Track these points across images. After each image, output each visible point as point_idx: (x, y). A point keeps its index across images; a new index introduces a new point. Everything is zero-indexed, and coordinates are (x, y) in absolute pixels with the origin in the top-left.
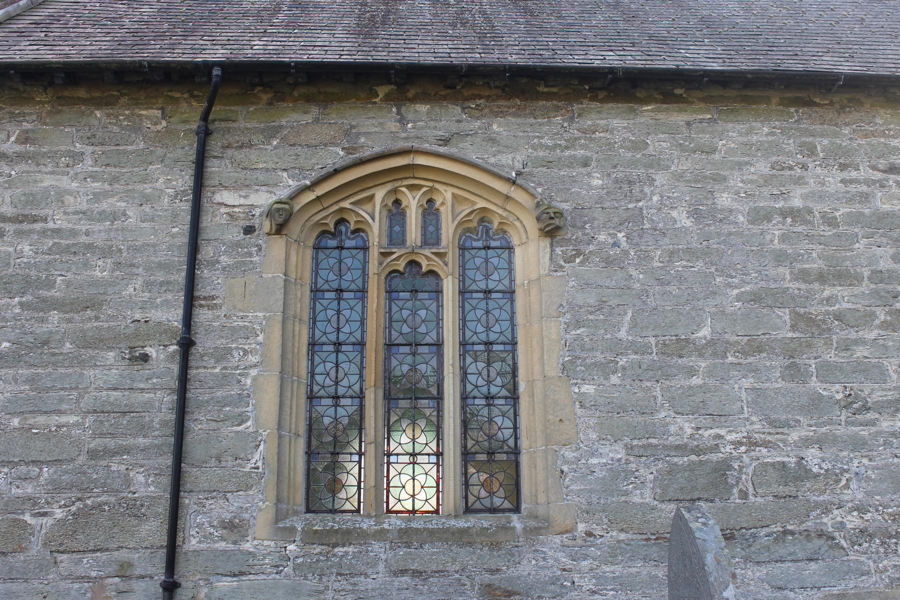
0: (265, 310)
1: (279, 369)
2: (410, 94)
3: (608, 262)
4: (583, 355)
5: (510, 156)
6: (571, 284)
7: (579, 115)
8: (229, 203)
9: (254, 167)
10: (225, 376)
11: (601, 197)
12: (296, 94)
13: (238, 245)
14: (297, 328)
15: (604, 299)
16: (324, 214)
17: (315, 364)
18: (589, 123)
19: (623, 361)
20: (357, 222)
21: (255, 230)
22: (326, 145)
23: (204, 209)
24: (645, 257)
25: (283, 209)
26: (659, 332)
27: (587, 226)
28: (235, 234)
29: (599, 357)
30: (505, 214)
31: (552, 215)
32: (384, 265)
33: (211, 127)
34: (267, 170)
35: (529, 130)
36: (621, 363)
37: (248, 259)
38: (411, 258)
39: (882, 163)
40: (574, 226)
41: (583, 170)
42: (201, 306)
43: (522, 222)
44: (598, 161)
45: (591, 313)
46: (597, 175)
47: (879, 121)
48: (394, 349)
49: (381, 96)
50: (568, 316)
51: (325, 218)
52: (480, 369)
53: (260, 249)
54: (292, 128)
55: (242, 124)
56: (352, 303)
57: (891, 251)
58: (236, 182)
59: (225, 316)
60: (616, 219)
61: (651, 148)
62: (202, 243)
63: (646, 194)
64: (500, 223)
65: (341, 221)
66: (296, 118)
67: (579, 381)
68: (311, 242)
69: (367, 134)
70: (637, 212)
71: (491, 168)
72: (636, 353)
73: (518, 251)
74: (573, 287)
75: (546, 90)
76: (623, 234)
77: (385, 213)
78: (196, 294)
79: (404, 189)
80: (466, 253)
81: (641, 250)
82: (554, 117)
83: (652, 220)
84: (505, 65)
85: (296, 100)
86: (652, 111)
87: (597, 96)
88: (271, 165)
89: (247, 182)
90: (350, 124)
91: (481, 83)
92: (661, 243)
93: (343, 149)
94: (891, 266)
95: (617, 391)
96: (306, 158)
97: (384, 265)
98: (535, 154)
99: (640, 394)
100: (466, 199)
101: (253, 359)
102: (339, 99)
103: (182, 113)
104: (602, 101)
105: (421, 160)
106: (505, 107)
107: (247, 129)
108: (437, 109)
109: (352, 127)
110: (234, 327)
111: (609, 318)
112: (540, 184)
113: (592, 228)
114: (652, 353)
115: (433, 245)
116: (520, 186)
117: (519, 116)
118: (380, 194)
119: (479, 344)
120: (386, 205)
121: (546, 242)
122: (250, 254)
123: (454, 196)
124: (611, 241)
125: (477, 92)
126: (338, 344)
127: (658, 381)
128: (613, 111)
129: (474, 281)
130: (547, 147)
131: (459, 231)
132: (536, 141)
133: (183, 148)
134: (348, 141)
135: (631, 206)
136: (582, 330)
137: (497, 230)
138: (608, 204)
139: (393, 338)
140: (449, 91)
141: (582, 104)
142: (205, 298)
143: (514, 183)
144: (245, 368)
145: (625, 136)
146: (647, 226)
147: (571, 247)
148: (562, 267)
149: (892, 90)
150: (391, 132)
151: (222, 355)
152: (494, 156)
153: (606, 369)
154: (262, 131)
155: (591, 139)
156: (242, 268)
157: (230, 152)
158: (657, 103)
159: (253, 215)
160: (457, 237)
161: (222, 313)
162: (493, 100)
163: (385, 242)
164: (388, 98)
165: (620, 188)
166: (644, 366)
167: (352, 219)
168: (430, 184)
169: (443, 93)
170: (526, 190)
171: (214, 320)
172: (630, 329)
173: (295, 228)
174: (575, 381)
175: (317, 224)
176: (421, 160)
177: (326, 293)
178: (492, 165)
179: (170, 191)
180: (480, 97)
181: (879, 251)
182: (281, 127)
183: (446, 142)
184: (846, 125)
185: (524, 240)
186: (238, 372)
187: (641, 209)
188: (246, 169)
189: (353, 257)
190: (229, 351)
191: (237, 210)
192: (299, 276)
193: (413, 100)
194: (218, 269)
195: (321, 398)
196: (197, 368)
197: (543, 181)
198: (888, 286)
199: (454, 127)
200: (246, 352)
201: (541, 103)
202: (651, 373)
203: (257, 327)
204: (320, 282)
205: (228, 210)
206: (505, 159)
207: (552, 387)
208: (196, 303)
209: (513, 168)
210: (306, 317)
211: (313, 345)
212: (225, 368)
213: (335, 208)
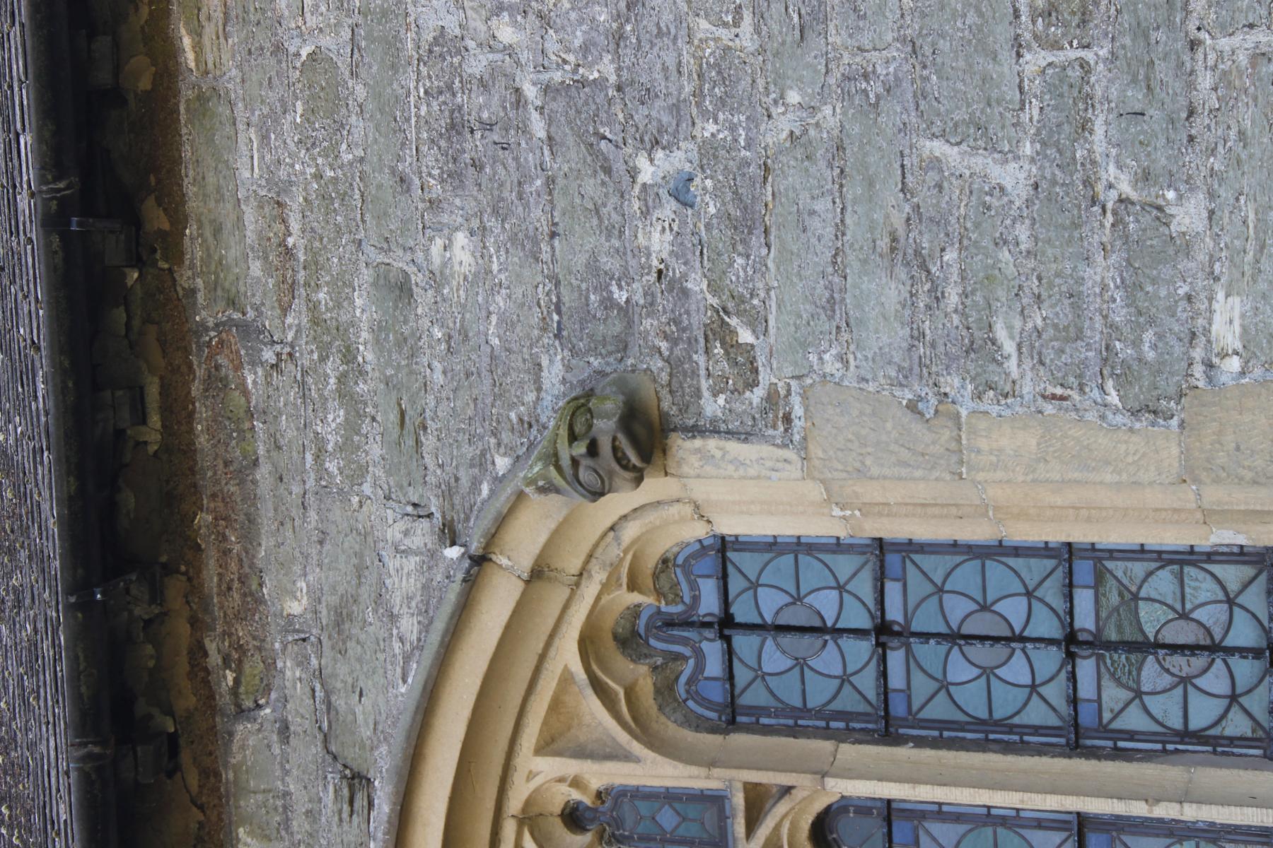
3: (746, 223)
4: (1095, 332)
5: (392, 563)
6: (831, 366)
7: (232, 303)
11: (513, 238)
15: (884, 244)
18: (256, 268)
19: (1119, 181)
24: (721, 79)
26: (1002, 34)
27: (621, 296)
29: (1102, 271)
30: (599, 574)
31: (580, 449)
35: (297, 489)
36: (1126, 188)
40: (623, 347)
41: (424, 300)
43: (624, 517)
44: (386, 245)
45: (937, 297)
46: (436, 248)
50: (951, 383)
52: (1167, 680)
60: (591, 187)
61: (327, 41)
63: (493, 69)
64: (633, 586)
67: (1198, 354)
70: (559, 105)
71: (440, 625)
72: (1085, 126)
73: (729, 526)
74: (842, 359)
75: (155, 420)
76: (642, 162)
80: (746, 700)
81: (698, 94)
82: (246, 393)
83: (585, 49)
84: (69, 608)
86: (197, 33)
87: (163, 235)
91: (149, 649)
92: (667, 17)
95: (1236, 208)
98: (380, 472)
99: (1247, 116)
100: (556, 705)
104: (179, 218)
106: (223, 565)
108: (249, 804)
111: (954, 228)
112: (482, 462)
113: (625, 278)
114: (1083, 64)
115: (723, 819)
116: (492, 538)
117: (251, 520)
119: (1073, 677)
121: (683, 448)
123: (546, 747)
124: (669, 208)
125: (183, 665)
127: (1194, 45)
128: (211, 179)
129: (845, 679)
130: (351, 427)
131: (672, 729)
132: (332, 466)
135: (538, 127)
136: (1001, 333)
137: (659, 593)
138: (537, 213)
140: (185, 757)
141: (193, 292)
143: (480, 561)
145: (292, 139)
146: (606, 68)
147: (700, 359)
148: (772, 398)
152: (393, 618)
153: (1148, 246)
155: (314, 265)
158: (167, 13)
160: (689, 736)
162: (206, 605)
165: (477, 165)
166: (1136, 98)
168: (509, 828)
169: (193, 780)
170: (502, 521)
172: (991, 147)
174: (1198, 370)
178: (426, 628)
180: (198, 651)
183: (357, 781)
185: (688, 509)
187: (547, 89)
197: (469, 451)
199: (307, 751)
201: (202, 441)
202: (1163, 71)
206: (403, 579)
207: (1221, 458)
209: (433, 555)
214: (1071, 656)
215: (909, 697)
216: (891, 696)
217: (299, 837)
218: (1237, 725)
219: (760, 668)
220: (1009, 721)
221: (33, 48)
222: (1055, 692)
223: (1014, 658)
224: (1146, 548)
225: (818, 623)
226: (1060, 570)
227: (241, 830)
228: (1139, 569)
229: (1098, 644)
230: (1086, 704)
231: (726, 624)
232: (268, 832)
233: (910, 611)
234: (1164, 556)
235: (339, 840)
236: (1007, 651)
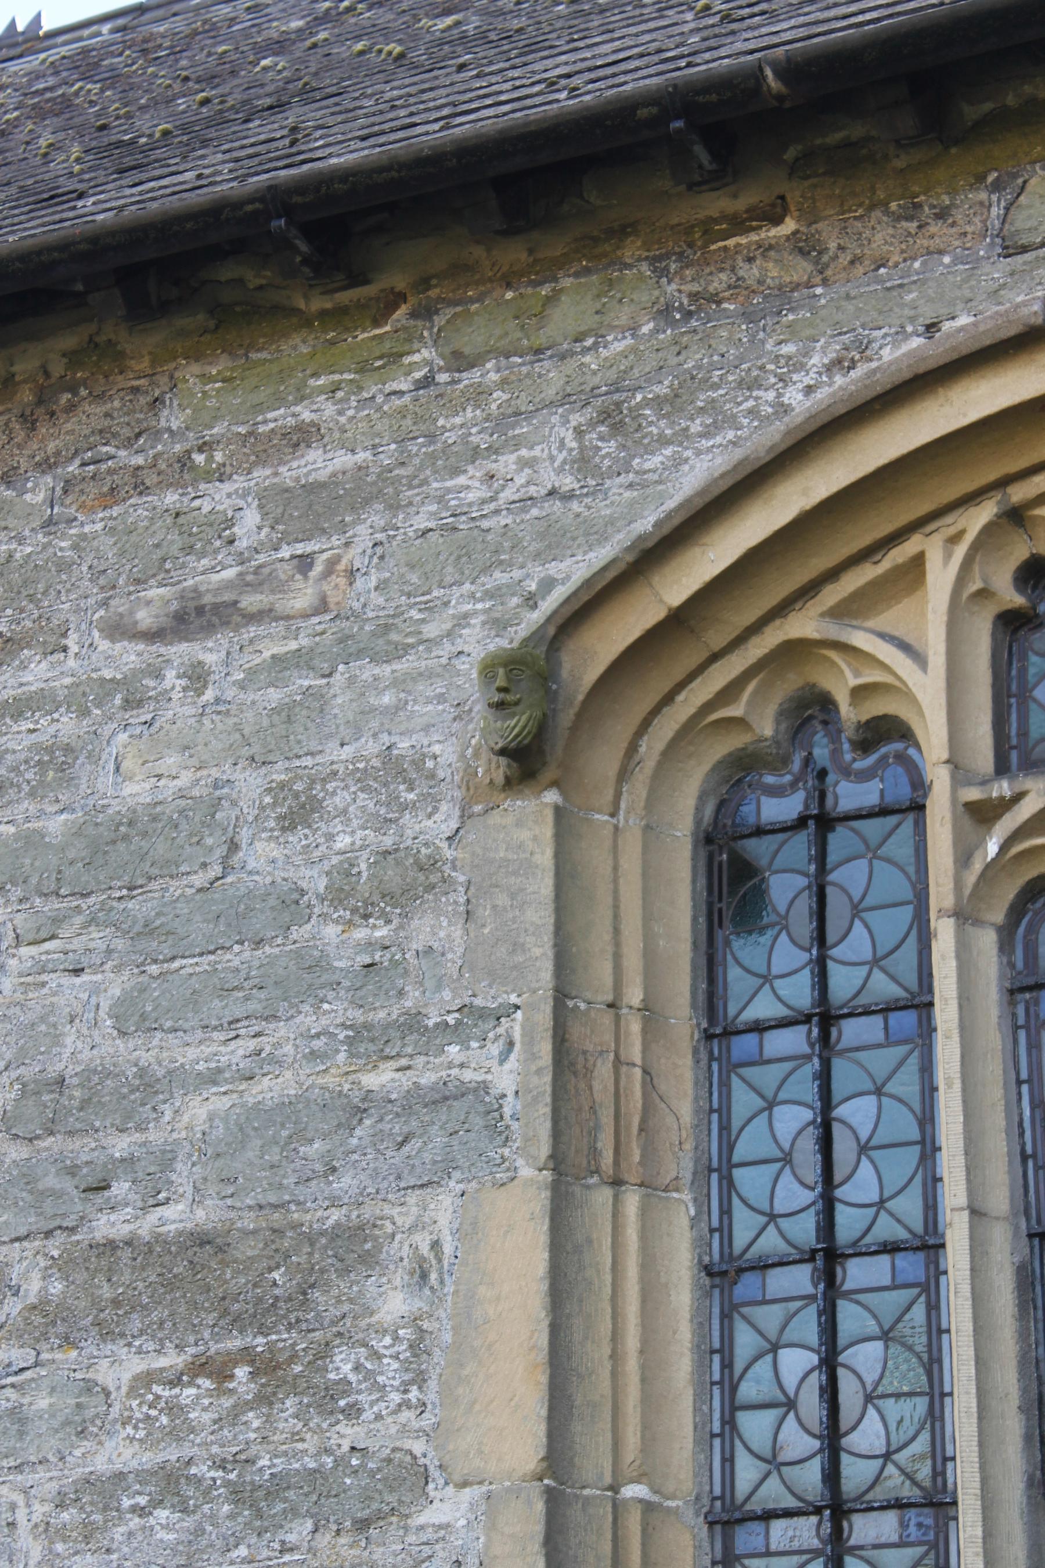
20: (860, 693)
39: (154, 602)
47: (173, 418)
51: (729, 693)
57: (116, 986)
65: (812, 709)
94: (106, 1049)
108: (542, 1387)
120: (984, 594)
126: (828, 1257)
139: (741, 1238)
149: (227, 272)
163: (984, 758)
167: (841, 682)
181: (70, 991)
184: (46, 465)
195: (768, 1516)
198: (77, 1143)
211: (725, 1274)
220: (729, 957)
222: (771, 1242)
223: (806, 1191)
224: (939, 1185)
226: (901, 993)
229: (829, 1279)
230: (759, 1284)
231: (821, 822)
233: (860, 1297)
234: (936, 1366)
236: (816, 1430)
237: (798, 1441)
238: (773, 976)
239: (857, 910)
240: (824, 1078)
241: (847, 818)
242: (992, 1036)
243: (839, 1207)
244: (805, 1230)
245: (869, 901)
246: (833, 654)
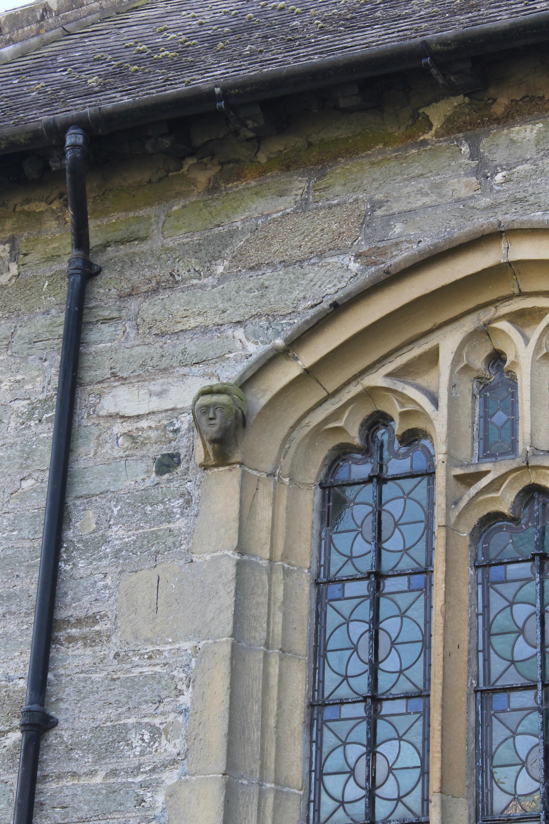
0: (197, 634)
1: (222, 767)
2: (498, 109)
8: (129, 412)
9: (180, 327)
10: (112, 791)
12: (262, 158)
13: (145, 499)
14: (274, 671)
16: (330, 408)
17: (325, 750)
20: (404, 415)
21: (179, 463)
22: (321, 255)
23: (83, 431)
25: (215, 406)
28: (139, 475)
32: (462, 504)
33: (98, 260)
34: (205, 330)
37: (165, 526)
38: (526, 481)
42: (71, 639)
48: (498, 700)
49: (437, 124)
52: (352, 761)
53: (188, 502)
54: (253, 232)
55: (157, 242)
56: (404, 600)
58: (143, 365)
59: (117, 655)
62: (74, 504)
65: (378, 420)
66: (265, 207)
68: (313, 470)
69: (406, 215)
77: (467, 387)
78: (61, 614)
79: (504, 325)
85: (262, 172)
88: (212, 319)
89: (164, 363)
90: (371, 201)
93: (358, 256)
96: (281, 291)
97: (462, 504)
101: (170, 747)
102: (350, 150)
103: (47, 242)
105: (525, 250)
107: (167, 250)
109: (376, 205)
110: (132, 680)
118: (449, 343)
120: (467, 368)
122: (168, 516)
133: (47, 312)
134: (367, 238)
142: (79, 622)
144: (153, 770)
150: (458, 200)
151: (109, 742)
154: (197, 249)
156: (152, 548)
157: (133, 305)
159: (176, 431)
161: (109, 650)
163: (468, 449)
164: (451, 128)
167: (394, 409)
171: (95, 667)
173: (264, 446)
175: (319, 432)
176: (525, 250)
177: (348, 585)
179: (21, 405)
182: (232, 234)
186: (139, 779)
188: (162, 334)
189: (406, 496)
190: (121, 734)
191: (144, 424)
192: (279, 552)
193: (507, 119)
194: (106, 556)
196: (59, 777)
200: (156, 733)
203: (179, 674)
204: (336, 560)
205: (126, 427)
208: (61, 635)
210: (301, 641)
211: (318, 707)
212: (114, 773)
213: (354, 390)
214: (365, 699)
215: (339, 599)
216: (502, 566)
217: (540, 164)
218: (327, 805)
219: (355, 504)
221: (387, 47)
222: (344, 692)
223: (359, 789)
225: (384, 538)
227: (541, 125)
228: (418, 740)
232: (541, 143)
235: (541, 191)
237: (357, 666)
238: (353, 545)
239: (396, 525)
240: (373, 730)
241: (395, 478)
242: (464, 591)
243: (377, 800)
244: (362, 685)
245: (399, 640)
246: (390, 394)
